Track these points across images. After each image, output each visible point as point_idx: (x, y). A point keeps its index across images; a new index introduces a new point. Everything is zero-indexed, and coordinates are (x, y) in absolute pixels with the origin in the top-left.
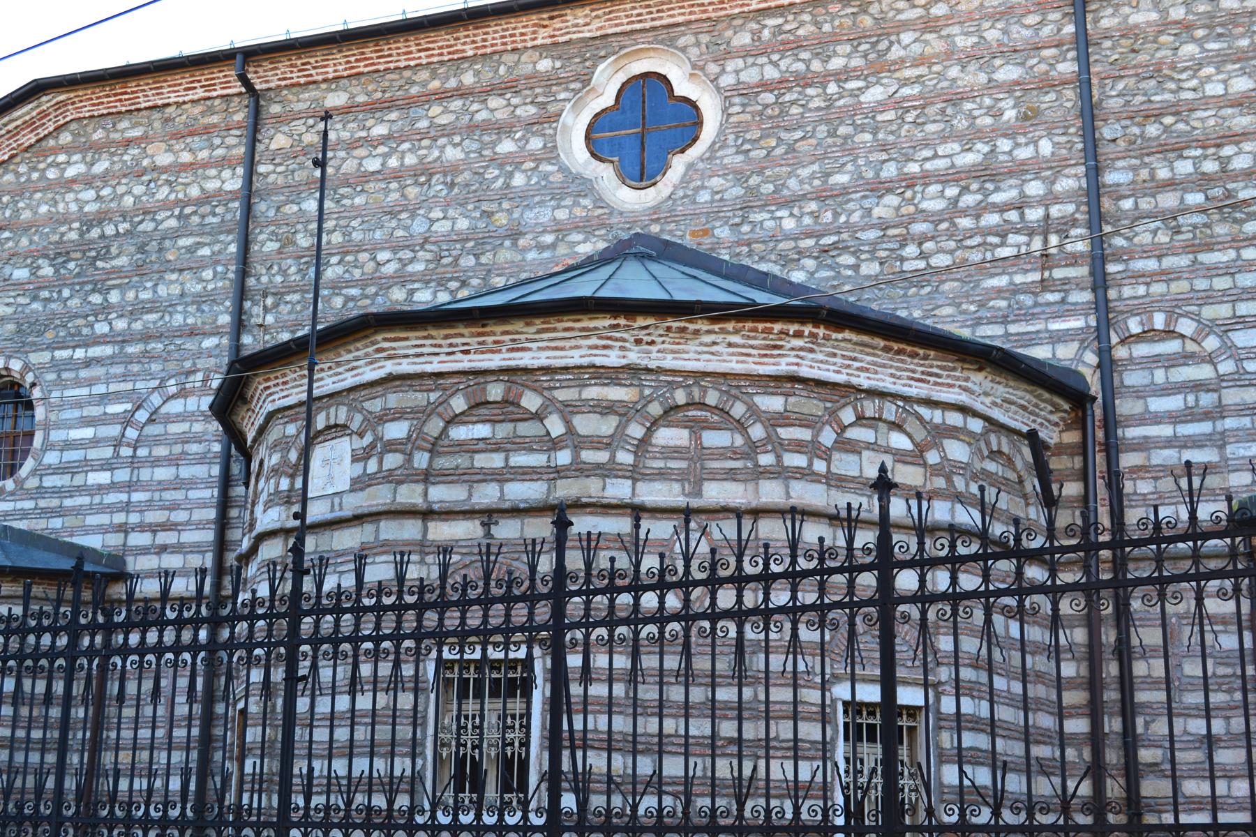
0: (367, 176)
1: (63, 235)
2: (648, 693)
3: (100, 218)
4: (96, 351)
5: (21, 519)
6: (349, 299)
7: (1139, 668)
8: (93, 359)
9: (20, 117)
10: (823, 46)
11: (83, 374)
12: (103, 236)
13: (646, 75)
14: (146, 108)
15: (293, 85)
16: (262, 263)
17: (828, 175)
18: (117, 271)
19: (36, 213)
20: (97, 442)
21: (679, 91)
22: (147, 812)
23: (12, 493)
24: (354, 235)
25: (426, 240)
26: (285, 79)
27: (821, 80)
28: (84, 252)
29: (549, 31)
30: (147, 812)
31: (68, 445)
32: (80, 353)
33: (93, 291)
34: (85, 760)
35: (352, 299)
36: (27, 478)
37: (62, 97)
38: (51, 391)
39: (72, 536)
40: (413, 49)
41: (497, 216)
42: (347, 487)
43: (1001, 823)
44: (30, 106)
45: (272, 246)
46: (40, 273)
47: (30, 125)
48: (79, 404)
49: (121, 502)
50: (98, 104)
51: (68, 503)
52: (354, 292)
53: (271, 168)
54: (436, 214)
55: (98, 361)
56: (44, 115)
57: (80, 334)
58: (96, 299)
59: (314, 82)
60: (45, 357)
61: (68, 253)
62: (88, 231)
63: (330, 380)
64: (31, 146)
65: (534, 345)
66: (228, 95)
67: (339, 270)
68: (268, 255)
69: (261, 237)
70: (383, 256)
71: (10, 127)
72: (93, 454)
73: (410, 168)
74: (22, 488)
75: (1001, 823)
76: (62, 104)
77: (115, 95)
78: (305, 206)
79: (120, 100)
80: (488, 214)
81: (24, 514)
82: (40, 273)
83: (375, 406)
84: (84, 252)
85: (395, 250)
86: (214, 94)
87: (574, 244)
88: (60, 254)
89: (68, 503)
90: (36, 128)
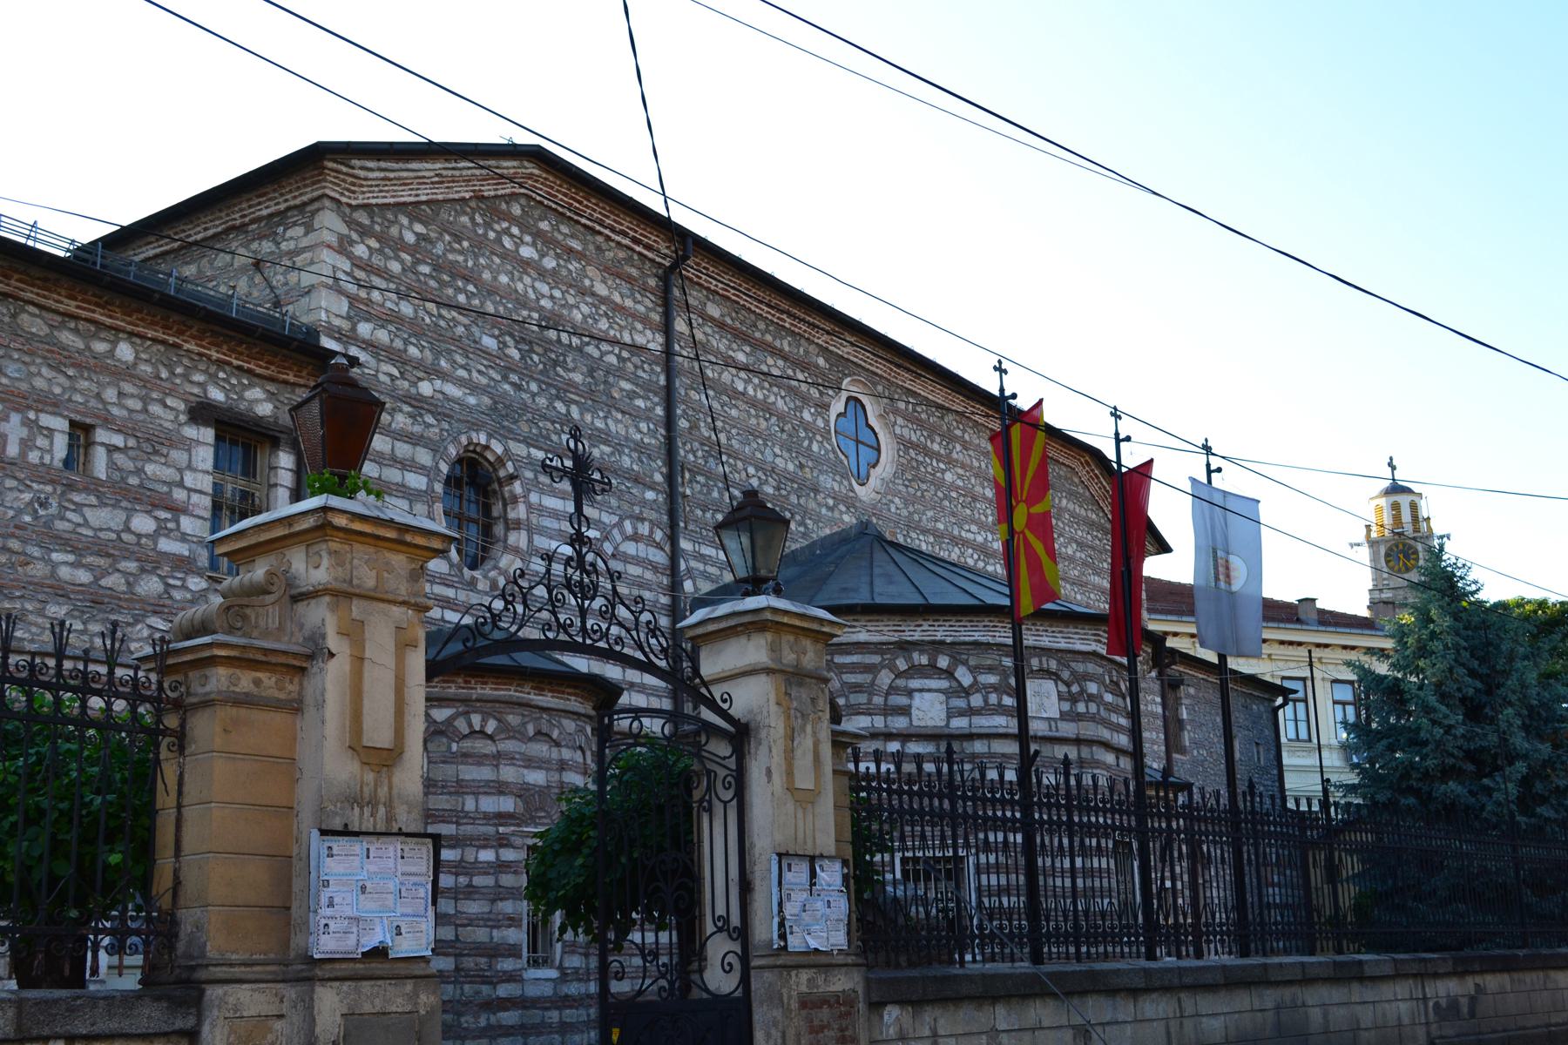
12: (559, 341)
28: (546, 350)
37: (536, 172)
42: (917, 695)
54: (777, 450)
80: (801, 466)
83: (1080, 667)
87: (841, 513)
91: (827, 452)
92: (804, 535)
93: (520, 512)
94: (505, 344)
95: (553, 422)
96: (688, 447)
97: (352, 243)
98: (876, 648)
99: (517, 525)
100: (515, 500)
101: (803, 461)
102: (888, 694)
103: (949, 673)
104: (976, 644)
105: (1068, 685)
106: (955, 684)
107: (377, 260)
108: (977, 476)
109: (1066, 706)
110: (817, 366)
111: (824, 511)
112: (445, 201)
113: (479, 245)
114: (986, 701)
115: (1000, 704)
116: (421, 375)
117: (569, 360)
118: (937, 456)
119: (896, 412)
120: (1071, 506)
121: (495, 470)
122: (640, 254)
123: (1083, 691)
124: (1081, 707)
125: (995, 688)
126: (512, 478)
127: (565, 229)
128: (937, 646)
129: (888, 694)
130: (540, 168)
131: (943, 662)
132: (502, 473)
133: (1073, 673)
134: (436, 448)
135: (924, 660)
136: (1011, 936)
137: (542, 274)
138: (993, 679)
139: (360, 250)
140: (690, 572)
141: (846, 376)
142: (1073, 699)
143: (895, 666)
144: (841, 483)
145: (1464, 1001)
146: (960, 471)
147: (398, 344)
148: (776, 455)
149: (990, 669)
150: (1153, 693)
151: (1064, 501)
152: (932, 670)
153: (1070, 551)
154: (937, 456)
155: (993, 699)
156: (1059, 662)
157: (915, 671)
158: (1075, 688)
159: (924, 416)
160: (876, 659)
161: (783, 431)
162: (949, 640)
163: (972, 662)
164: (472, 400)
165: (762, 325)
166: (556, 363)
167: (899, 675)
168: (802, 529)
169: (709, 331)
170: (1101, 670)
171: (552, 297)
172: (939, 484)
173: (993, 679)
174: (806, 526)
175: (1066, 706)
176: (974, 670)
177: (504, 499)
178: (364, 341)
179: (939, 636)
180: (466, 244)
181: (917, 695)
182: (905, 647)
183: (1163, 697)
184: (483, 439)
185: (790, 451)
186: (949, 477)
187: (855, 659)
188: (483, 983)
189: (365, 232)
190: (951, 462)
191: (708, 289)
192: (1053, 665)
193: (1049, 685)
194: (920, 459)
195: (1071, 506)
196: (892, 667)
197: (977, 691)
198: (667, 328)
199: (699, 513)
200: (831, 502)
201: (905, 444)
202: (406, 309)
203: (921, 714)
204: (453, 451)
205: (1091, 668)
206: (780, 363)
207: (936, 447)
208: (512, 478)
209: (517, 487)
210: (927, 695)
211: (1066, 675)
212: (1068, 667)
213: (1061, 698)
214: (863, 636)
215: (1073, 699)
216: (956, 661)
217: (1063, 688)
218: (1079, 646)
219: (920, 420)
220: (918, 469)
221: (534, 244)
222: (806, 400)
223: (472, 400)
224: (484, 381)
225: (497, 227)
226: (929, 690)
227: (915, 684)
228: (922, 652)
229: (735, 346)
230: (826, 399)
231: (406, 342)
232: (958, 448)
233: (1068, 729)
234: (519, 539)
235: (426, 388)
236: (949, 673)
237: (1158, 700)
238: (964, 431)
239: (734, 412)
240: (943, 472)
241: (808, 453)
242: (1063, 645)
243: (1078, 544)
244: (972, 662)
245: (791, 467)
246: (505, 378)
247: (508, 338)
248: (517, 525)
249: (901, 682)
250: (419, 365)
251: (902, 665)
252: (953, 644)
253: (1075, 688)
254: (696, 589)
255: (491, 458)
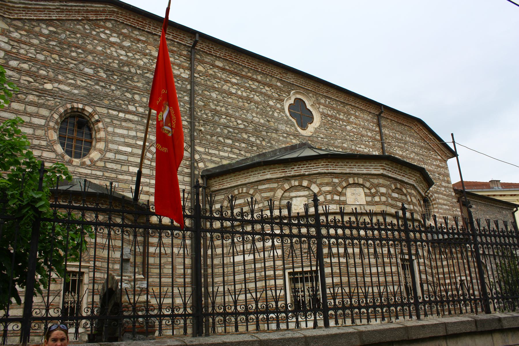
0: (231, 94)
1: (110, 63)
2: (270, 273)
3: (128, 64)
4: (128, 116)
5: (95, 179)
6: (229, 132)
7: (216, 271)
8: (128, 119)
9: (96, 7)
10: (339, 111)
11: (124, 124)
12: (130, 71)
13: (300, 99)
14: (147, 32)
15: (204, 52)
16: (198, 108)
17: (343, 143)
18: (138, 88)
19: (95, 48)
20: (134, 155)
21: (308, 107)
22: (396, 309)
23: (90, 166)
24: (229, 111)
25: (252, 122)
26: (202, 48)
27: (336, 119)
28: (121, 74)
29: (281, 76)
30: (396, 309)
31: (118, 152)
32: (121, 115)
33: (127, 91)
34: (480, 287)
35: (230, 132)
36: (97, 161)
37: (116, 10)
38: (108, 126)
39: (123, 192)
40: (246, 61)
41: (271, 123)
42: (294, 199)
43: (187, 313)
44: (102, 5)
45: (201, 103)
46: (99, 74)
47: (96, 12)
48: (123, 136)
49: (147, 182)
50: (128, 20)
51: (120, 177)
52: (231, 130)
53: (198, 76)
54: (254, 115)
55: (131, 121)
56: (104, 11)
57: (121, 107)
58: (129, 95)
59: (212, 55)
60: (105, 111)
61: (113, 71)
62: (123, 66)
63: (356, 169)
64: (92, 20)
65: (406, 176)
66: (181, 43)
67: (225, 121)
68: (200, 106)
69: (197, 99)
70: (239, 122)
71: (89, 8)
72: (131, 159)
73: (244, 97)
74: (94, 165)
75: (187, 313)
76: (114, 12)
77: (137, 20)
78: (212, 94)
79: (138, 23)
80: (268, 121)
81: (97, 177)
82: (99, 74)
83: (376, 181)
84: (121, 74)
85: (243, 121)
86: (176, 40)
87: (291, 139)
88: (109, 70)
89: (120, 177)
90: (97, 15)
91: (283, 116)
92: (270, 147)
93: (102, 134)
94: (98, 72)
95: (124, 101)
96: (203, 112)
97: (10, 32)
98: (276, 180)
99: (100, 140)
100: (99, 130)
101: (269, 119)
102: (281, 200)
103: (308, 188)
104: (320, 174)
105: (369, 189)
106: (311, 193)
107: (24, 39)
108: (363, 128)
109: (369, 199)
110: (277, 86)
111: (281, 138)
112: (66, 20)
113: (85, 36)
114: (325, 198)
115: (332, 199)
116: (46, 81)
117: (135, 78)
118: (343, 120)
119: (320, 104)
120: (411, 140)
121: (90, 119)
122: (178, 42)
123: (377, 192)
124: (377, 199)
125: (329, 192)
126: (98, 121)
127: (136, 33)
128: (302, 176)
129: (281, 200)
130: (117, 8)
131: (305, 183)
132: (93, 120)
133: (372, 184)
134: (51, 109)
135: (297, 183)
136: (459, 301)
137: (122, 48)
138: (328, 188)
139: (15, 35)
140: (202, 160)
141: (293, 90)
142: (373, 195)
143: (284, 187)
144: (290, 128)
145: (342, 198)
146: (354, 126)
147: (34, 69)
148: (254, 117)
149: (327, 184)
150: (456, 207)
151: (408, 139)
152: (301, 187)
153: (412, 156)
154: (343, 120)
155: (329, 197)
156: (364, 179)
157: (292, 188)
158: (373, 191)
159: (334, 106)
160: (275, 185)
161: (257, 108)
162: (307, 173)
163: (318, 182)
164: (76, 92)
165: (246, 70)
166: (126, 79)
167: (286, 191)
168: (269, 145)
169: (216, 71)
170: (389, 183)
171: (127, 56)
172: (343, 130)
173: (328, 188)
174: (271, 144)
175: (369, 199)
176: (320, 185)
177: (95, 130)
178: (12, 68)
179: (302, 172)
180: (78, 35)
181: (294, 199)
182: (287, 179)
183: (461, 209)
184: (80, 106)
185: (261, 115)
186: (348, 128)
187: (266, 186)
188: (36, 336)
189: (17, 29)
190: (349, 123)
191: (216, 56)
192: (361, 181)
193: (360, 190)
194: (333, 120)
195: (411, 140)
196: (282, 188)
197: (321, 194)
198: (192, 69)
199: (209, 137)
200: (285, 135)
201: (322, 114)
202: (41, 57)
203: (296, 207)
204: (62, 110)
205: (381, 181)
206: (256, 84)
207: (341, 117)
208: (98, 121)
209: (100, 125)
210: (299, 199)
211: (368, 184)
212: (369, 181)
213: (366, 195)
214: (269, 176)
215: (373, 195)
216: (311, 182)
217: (367, 191)
218: (373, 172)
219: (333, 107)
220: (332, 124)
221: (118, 37)
222: (270, 97)
223: (76, 92)
224: (84, 84)
225: (97, 30)
226: (300, 196)
227: (293, 194)
228: (295, 180)
229: (231, 77)
230: (282, 98)
231: (39, 69)
232: (353, 117)
233: (368, 208)
234: (101, 145)
235: (49, 86)
236: (308, 188)
237: (459, 210)
238: (356, 112)
239: (230, 100)
240: (346, 126)
241: (272, 116)
242: (365, 171)
243: (416, 154)
244: (318, 182)
245: (262, 121)
246: (97, 84)
247: (99, 69)
248: (100, 140)
249: (287, 194)
250: (44, 77)
251: (287, 186)
252: (309, 175)
253: (373, 191)
254: (206, 166)
255: (88, 114)
